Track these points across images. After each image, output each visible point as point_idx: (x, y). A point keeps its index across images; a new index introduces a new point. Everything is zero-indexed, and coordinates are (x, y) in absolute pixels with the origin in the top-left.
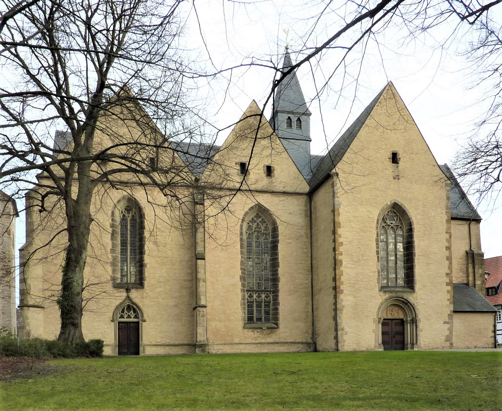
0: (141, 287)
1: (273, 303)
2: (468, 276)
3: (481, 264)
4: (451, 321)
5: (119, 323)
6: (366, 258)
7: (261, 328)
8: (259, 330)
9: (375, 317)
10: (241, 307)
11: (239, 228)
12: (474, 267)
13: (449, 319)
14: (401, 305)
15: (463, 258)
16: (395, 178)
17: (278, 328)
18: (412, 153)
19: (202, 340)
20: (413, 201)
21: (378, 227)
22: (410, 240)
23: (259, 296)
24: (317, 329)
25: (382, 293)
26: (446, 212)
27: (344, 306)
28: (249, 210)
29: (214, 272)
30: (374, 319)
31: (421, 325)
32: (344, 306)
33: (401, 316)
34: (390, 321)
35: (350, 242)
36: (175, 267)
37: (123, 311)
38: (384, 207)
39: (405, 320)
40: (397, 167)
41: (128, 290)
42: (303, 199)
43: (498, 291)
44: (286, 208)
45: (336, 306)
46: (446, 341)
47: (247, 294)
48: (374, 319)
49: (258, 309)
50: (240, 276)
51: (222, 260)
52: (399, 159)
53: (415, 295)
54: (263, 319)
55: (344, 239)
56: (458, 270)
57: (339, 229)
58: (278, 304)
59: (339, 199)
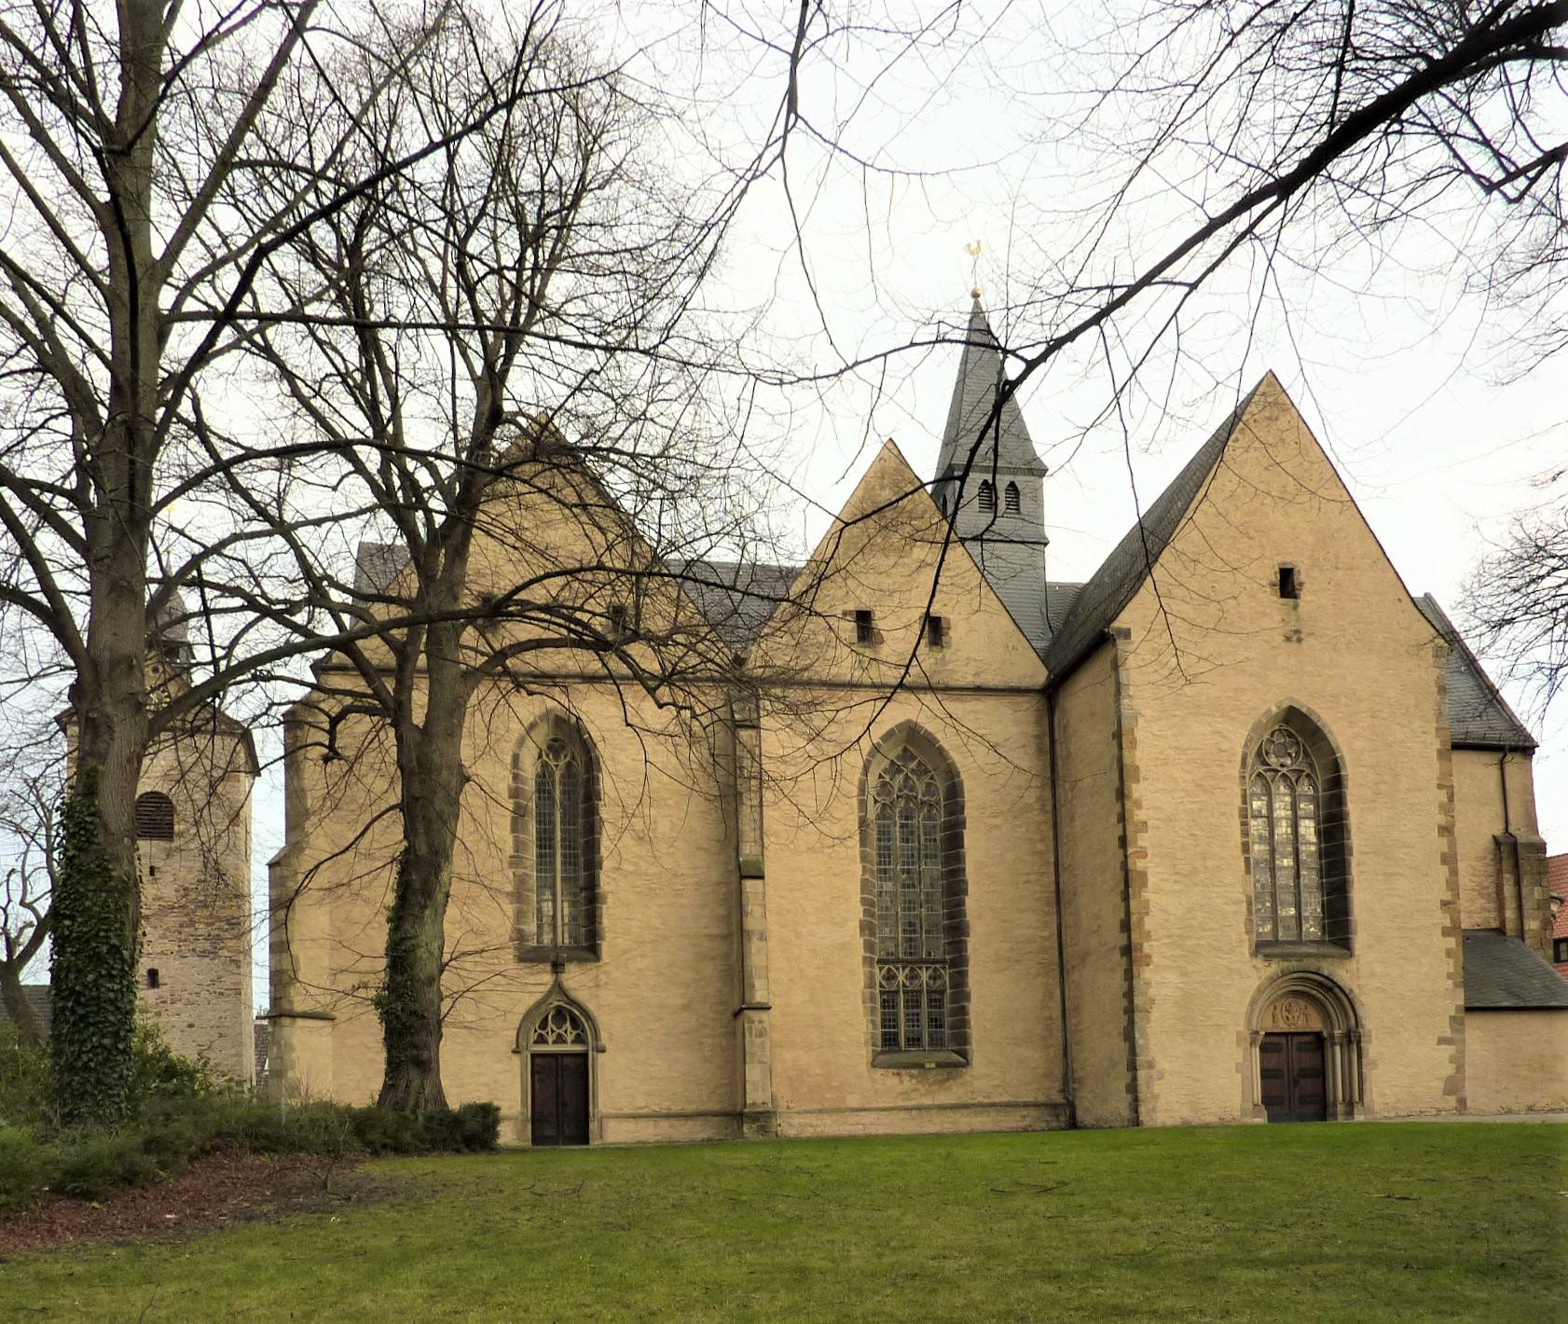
0: (592, 956)
1: (952, 995)
2: (1501, 908)
3: (1539, 873)
4: (1458, 1036)
5: (534, 1056)
7: (921, 1066)
8: (914, 1072)
9: (1242, 1029)
11: (855, 791)
12: (1518, 883)
13: (1453, 1029)
15: (1485, 858)
16: (1288, 639)
17: (967, 1064)
18: (1337, 568)
19: (759, 1102)
20: (1343, 700)
22: (1335, 810)
25: (1259, 962)
26: (1437, 729)
27: (1153, 1001)
29: (789, 911)
30: (1238, 1033)
31: (1372, 1049)
32: (1153, 1001)
33: (1316, 1024)
34: (1283, 1040)
35: (1169, 820)
36: (683, 901)
37: (544, 1025)
38: (1260, 721)
40: (1296, 607)
41: (557, 967)
45: (1131, 1002)
46: (1447, 1092)
48: (1238, 1033)
49: (911, 1011)
50: (861, 921)
52: (1301, 584)
53: (1352, 965)
54: (926, 1038)
55: (1150, 812)
56: (1473, 890)
58: (967, 997)
59: (1134, 702)
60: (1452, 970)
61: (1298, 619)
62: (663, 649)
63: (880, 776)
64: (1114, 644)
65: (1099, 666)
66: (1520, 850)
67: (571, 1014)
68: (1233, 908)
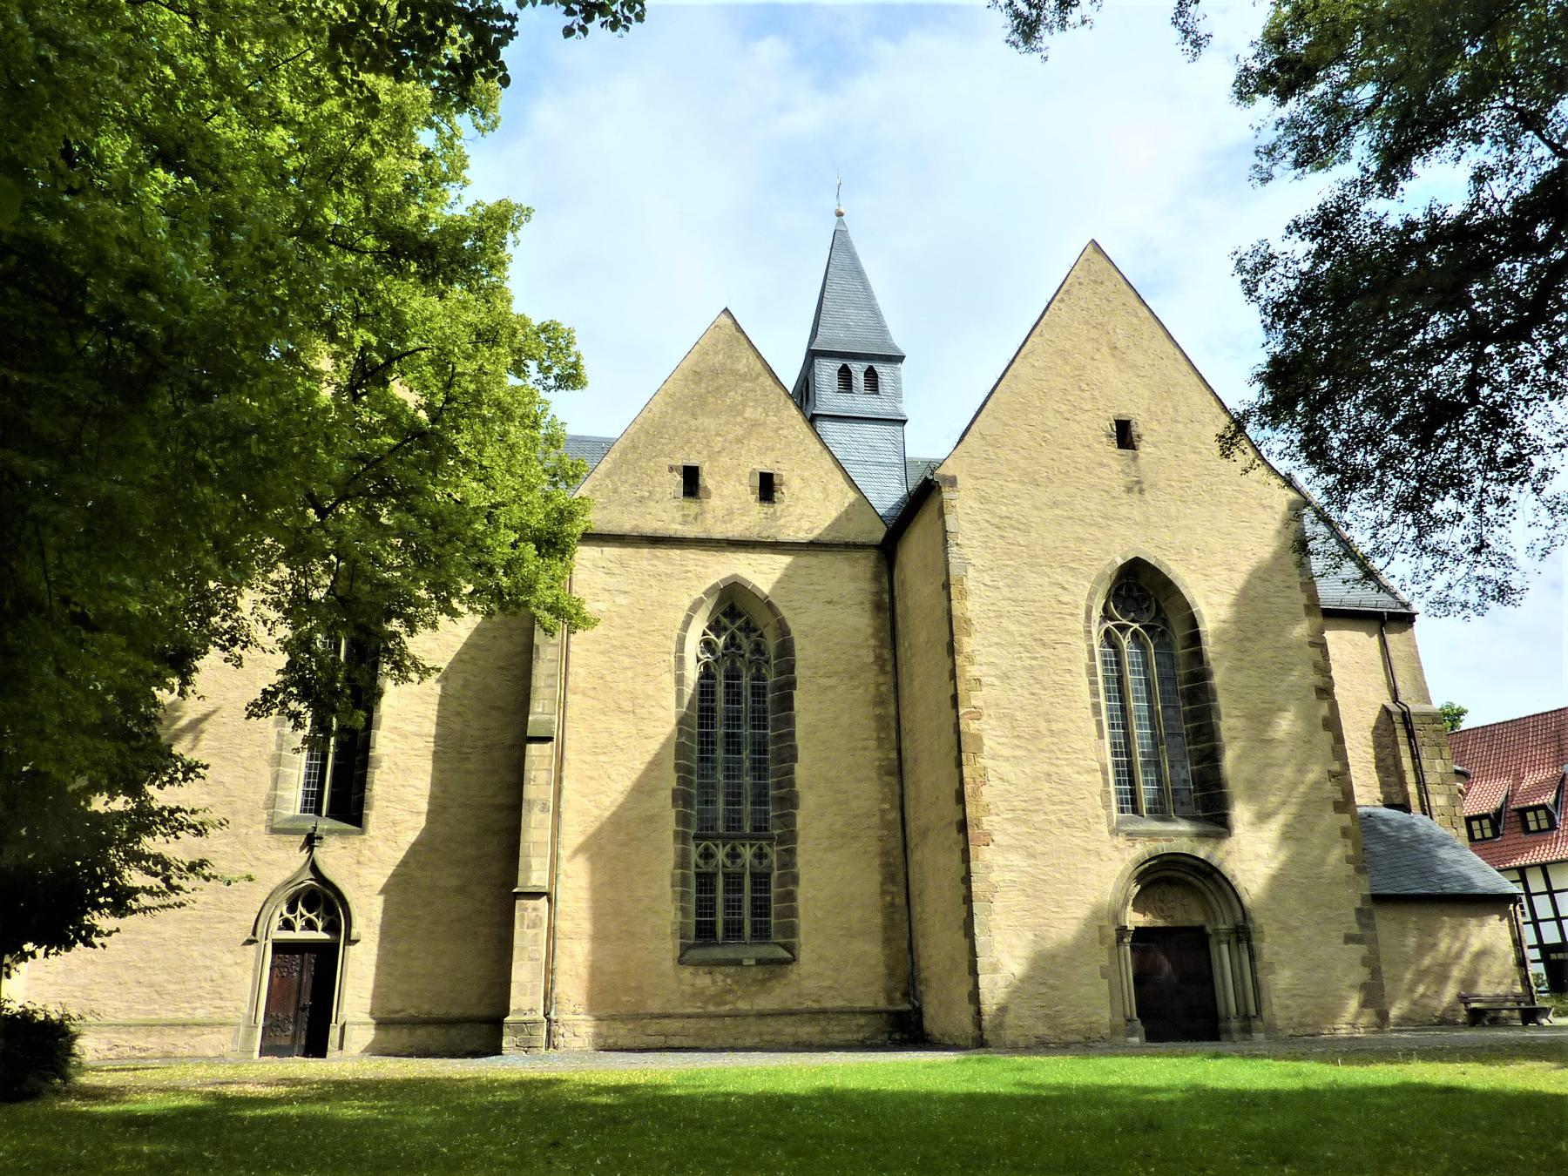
1: (780, 876)
5: (279, 947)
6: (1061, 726)
7: (738, 963)
8: (732, 970)
10: (674, 892)
11: (673, 647)
13: (1362, 925)
14: (1190, 878)
16: (1129, 490)
17: (794, 960)
21: (1090, 632)
22: (1196, 669)
23: (734, 855)
24: (922, 964)
25: (1121, 840)
27: (995, 888)
28: (704, 593)
31: (1267, 948)
32: (995, 888)
33: (1197, 919)
35: (1005, 677)
36: (469, 766)
38: (1104, 573)
39: (1209, 929)
40: (1135, 458)
42: (864, 565)
43: (1501, 827)
44: (818, 588)
45: (969, 888)
47: (697, 846)
49: (731, 896)
50: (674, 791)
51: (620, 743)
53: (1228, 844)
55: (984, 668)
57: (965, 639)
58: (795, 879)
60: (1351, 853)
61: (1138, 470)
62: (1073, 705)
63: (704, 634)
64: (940, 492)
65: (927, 517)
66: (1414, 720)
67: (326, 896)
68: (1089, 778)
